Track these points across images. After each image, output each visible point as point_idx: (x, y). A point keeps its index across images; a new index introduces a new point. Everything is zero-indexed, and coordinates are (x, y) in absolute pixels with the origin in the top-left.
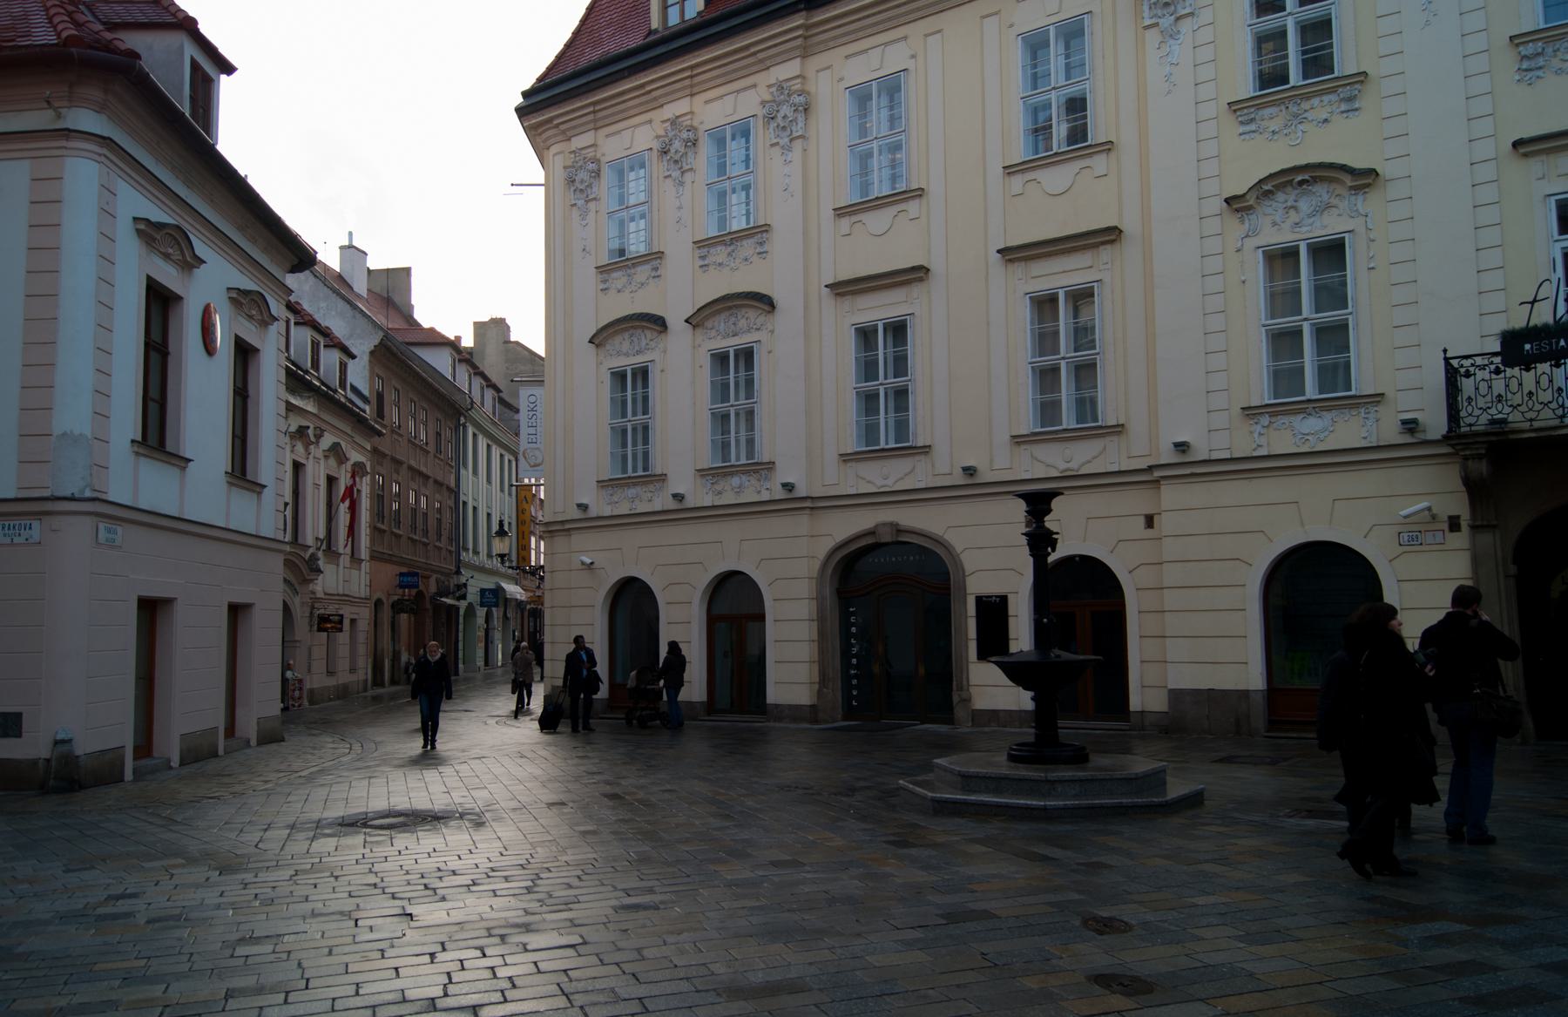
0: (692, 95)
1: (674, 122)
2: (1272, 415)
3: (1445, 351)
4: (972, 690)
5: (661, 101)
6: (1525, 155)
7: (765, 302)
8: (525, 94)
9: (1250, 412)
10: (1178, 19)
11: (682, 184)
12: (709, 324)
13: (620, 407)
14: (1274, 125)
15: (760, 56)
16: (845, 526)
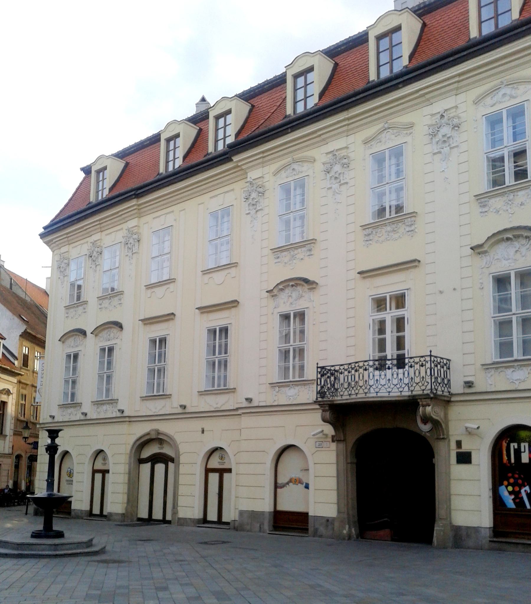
0: (102, 231)
1: (93, 243)
2: (279, 387)
3: (317, 364)
4: (179, 508)
5: (91, 233)
6: (364, 278)
7: (119, 326)
8: (45, 228)
9: (273, 385)
10: (257, 211)
11: (96, 271)
12: (100, 335)
13: (152, 358)
14: (286, 260)
15: (123, 216)
16: (141, 430)
